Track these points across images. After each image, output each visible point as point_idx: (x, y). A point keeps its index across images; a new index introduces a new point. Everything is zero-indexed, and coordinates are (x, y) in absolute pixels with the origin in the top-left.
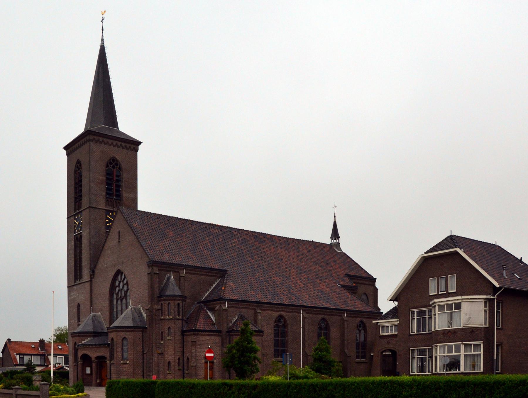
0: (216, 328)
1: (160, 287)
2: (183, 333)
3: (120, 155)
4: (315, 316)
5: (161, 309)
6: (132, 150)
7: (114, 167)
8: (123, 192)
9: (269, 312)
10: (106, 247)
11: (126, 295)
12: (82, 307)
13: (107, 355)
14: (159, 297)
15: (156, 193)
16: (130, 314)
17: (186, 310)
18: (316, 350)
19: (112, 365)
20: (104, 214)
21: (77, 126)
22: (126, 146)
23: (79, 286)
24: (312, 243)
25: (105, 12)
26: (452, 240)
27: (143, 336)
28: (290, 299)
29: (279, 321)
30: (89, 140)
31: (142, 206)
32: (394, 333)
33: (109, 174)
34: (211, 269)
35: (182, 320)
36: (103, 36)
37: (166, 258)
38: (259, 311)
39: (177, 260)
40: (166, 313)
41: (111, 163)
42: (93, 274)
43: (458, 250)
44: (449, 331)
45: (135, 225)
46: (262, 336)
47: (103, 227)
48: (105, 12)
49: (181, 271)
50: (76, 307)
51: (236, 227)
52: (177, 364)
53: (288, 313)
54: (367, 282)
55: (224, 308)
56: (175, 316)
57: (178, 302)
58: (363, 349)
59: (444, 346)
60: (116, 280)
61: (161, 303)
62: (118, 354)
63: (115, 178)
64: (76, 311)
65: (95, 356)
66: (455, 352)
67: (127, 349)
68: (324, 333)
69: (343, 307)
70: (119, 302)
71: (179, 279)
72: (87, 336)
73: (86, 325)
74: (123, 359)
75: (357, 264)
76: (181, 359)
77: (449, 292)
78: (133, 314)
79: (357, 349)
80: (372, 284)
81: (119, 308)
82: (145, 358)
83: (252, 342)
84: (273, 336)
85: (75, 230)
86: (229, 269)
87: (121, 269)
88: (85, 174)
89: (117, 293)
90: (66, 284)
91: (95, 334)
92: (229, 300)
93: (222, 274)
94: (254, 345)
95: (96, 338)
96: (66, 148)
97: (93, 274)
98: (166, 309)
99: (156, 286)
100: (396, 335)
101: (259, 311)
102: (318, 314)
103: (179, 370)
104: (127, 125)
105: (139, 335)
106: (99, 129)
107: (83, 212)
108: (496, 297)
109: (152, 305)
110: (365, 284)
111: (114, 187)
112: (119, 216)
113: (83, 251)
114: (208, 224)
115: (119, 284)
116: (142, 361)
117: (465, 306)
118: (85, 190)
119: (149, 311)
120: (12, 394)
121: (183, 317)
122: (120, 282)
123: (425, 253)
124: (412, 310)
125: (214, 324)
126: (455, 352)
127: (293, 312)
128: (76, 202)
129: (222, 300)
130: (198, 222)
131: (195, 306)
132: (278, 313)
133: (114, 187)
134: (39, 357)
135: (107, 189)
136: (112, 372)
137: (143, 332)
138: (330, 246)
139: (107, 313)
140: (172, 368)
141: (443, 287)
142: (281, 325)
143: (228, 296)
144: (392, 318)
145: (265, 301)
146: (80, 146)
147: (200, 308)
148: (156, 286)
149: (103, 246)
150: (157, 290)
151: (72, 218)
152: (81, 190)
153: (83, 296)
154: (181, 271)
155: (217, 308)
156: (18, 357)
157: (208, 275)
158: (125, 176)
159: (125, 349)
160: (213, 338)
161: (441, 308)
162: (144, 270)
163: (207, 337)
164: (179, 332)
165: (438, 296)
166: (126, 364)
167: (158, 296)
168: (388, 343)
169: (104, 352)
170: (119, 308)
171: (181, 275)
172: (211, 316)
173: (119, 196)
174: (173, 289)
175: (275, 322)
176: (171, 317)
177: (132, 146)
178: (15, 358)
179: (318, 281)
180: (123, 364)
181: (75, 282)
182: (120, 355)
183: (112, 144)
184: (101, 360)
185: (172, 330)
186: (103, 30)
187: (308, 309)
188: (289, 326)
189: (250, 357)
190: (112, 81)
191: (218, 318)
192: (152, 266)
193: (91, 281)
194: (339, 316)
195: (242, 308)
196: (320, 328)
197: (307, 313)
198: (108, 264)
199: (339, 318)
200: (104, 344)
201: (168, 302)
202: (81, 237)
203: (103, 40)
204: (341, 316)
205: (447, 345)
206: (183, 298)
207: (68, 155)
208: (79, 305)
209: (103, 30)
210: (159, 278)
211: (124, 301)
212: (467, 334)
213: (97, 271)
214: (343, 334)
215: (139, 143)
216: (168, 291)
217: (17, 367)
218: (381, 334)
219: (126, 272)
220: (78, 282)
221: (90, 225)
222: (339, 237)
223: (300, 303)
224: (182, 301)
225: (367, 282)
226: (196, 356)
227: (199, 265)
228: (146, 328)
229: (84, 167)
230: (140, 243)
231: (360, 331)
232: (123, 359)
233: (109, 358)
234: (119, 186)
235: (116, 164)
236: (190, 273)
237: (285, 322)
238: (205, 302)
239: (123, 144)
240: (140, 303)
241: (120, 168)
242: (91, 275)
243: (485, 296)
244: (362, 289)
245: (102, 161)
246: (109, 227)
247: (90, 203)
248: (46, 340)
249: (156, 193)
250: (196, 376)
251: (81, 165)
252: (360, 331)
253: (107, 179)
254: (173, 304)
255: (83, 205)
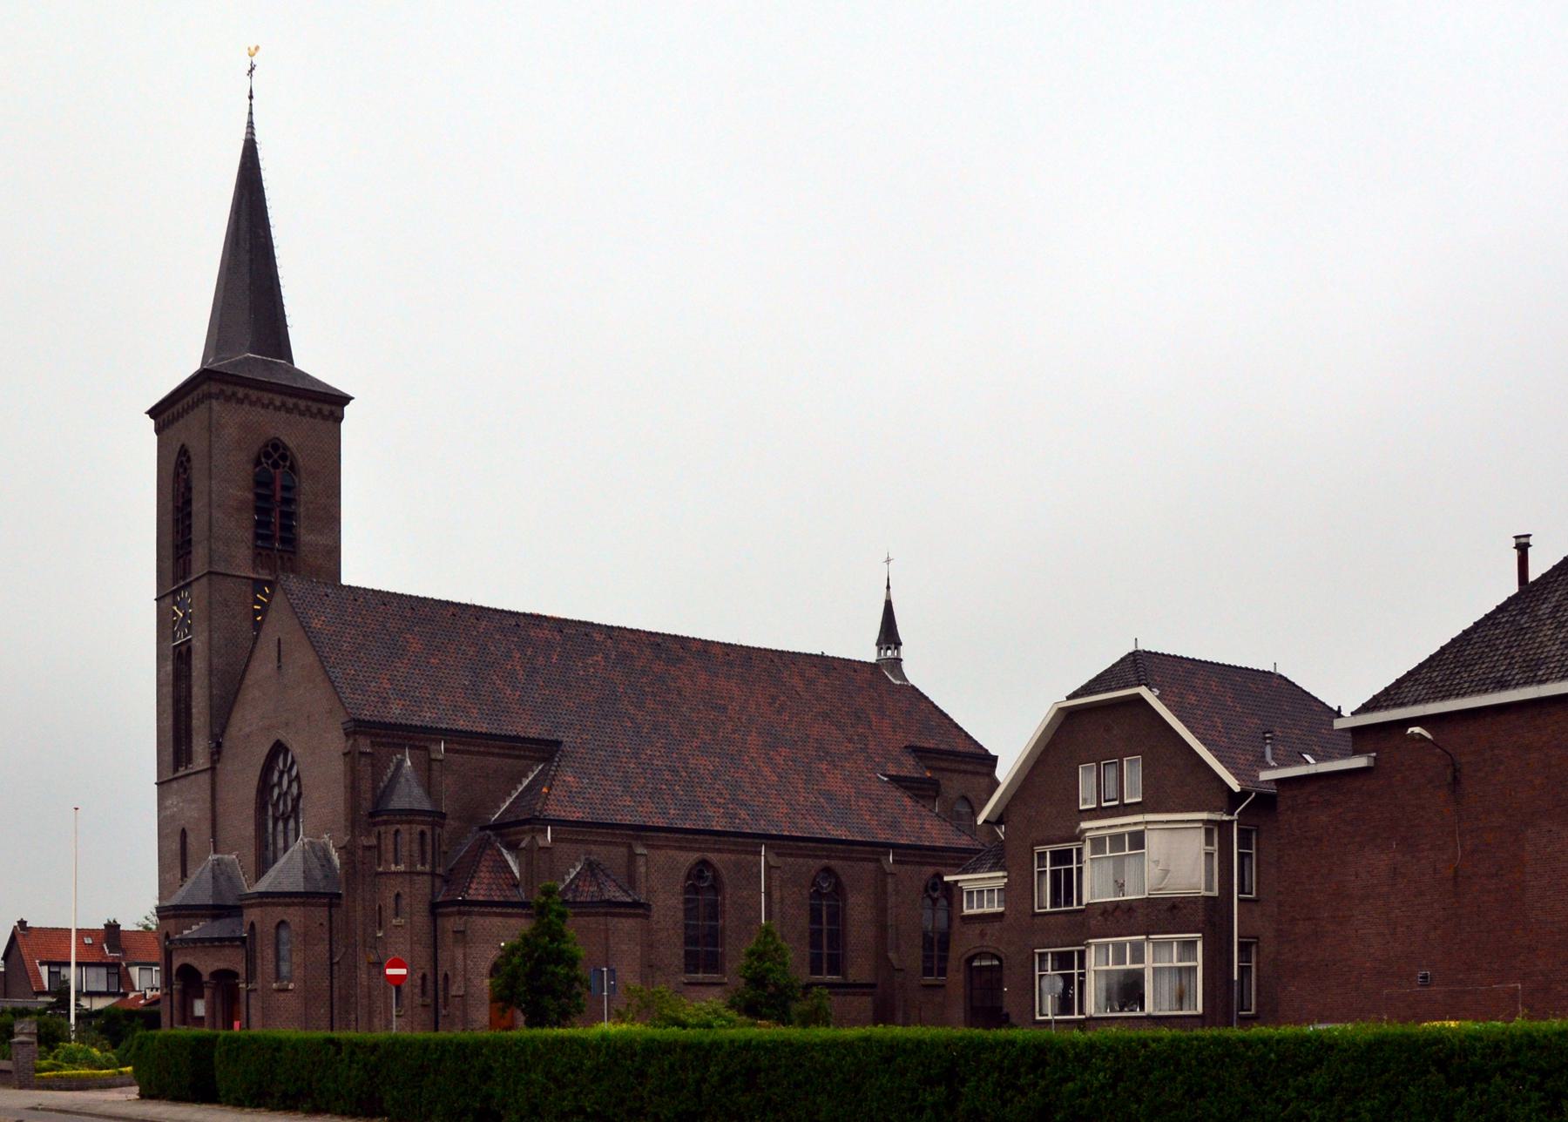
0: (520, 895)
1: (374, 789)
2: (435, 909)
3: (293, 432)
4: (801, 860)
5: (378, 847)
6: (325, 418)
7: (275, 465)
8: (302, 531)
9: (671, 853)
10: (247, 682)
11: (295, 808)
12: (191, 839)
13: (241, 969)
14: (371, 815)
15: (394, 534)
16: (298, 858)
17: (444, 848)
18: (751, 954)
19: (252, 995)
20: (249, 590)
21: (181, 354)
22: (308, 409)
23: (183, 782)
24: (822, 658)
25: (257, 48)
26: (1139, 665)
27: (331, 916)
28: (735, 816)
29: (700, 877)
30: (209, 396)
31: (358, 570)
32: (997, 909)
33: (262, 483)
34: (517, 738)
35: (433, 874)
36: (251, 113)
37: (395, 712)
38: (640, 850)
39: (427, 717)
40: (390, 856)
41: (268, 455)
42: (217, 751)
43: (1143, 691)
44: (1117, 905)
45: (316, 624)
46: (647, 917)
47: (247, 625)
48: (257, 48)
49: (433, 747)
50: (178, 839)
51: (603, 622)
52: (417, 991)
53: (726, 856)
54: (970, 768)
55: (541, 843)
56: (412, 864)
57: (419, 828)
58: (937, 947)
59: (1107, 945)
60: (273, 769)
61: (376, 830)
62: (265, 965)
63: (278, 496)
64: (177, 851)
65: (210, 970)
66: (1133, 962)
67: (290, 951)
68: (829, 906)
69: (882, 837)
70: (281, 825)
71: (427, 768)
72: (196, 916)
73: (197, 889)
74: (278, 978)
75: (946, 716)
76: (430, 977)
77: (1127, 801)
78: (305, 860)
79: (924, 948)
80: (985, 770)
81: (281, 843)
82: (336, 974)
83: (563, 936)
84: (681, 915)
85: (174, 634)
86: (566, 738)
87: (283, 740)
88: (199, 485)
89: (275, 805)
90: (152, 776)
91: (217, 911)
92: (557, 823)
93: (547, 750)
94: (564, 946)
95: (217, 923)
96: (153, 413)
97: (217, 751)
98: (391, 847)
99: (365, 785)
100: (1001, 914)
101: (640, 850)
102: (809, 856)
103: (424, 1006)
104: (314, 353)
105: (320, 914)
106: (236, 365)
107: (195, 586)
108: (1236, 816)
109: (353, 836)
110: (965, 772)
111: (275, 519)
112: (279, 597)
113: (195, 690)
114: (524, 615)
115: (281, 777)
116: (328, 983)
117: (1153, 840)
118: (199, 524)
119: (347, 851)
120: (9, 1072)
121: (433, 866)
122: (281, 774)
123: (1069, 698)
124: (1038, 849)
125: (516, 886)
126: (1133, 962)
127: (739, 852)
128: (177, 558)
129: (538, 822)
130: (496, 610)
131: (469, 840)
132: (693, 857)
133: (275, 519)
134: (103, 971)
135: (258, 524)
136: (252, 1011)
137: (331, 906)
138: (874, 668)
139: (251, 858)
140: (406, 1002)
141: (1111, 791)
142: (703, 885)
143: (554, 810)
144: (990, 870)
145: (661, 822)
146: (186, 411)
147: (485, 844)
148: (365, 785)
149: (242, 678)
150: (369, 796)
151: (169, 600)
152: (189, 526)
153: (193, 811)
154: (433, 747)
155: (523, 845)
156: (44, 971)
157: (509, 756)
158: (307, 489)
159: (284, 950)
160: (512, 921)
161: (1098, 844)
162: (335, 742)
163: (498, 921)
164: (422, 908)
165: (1099, 813)
166: (287, 990)
167: (370, 812)
168: (982, 935)
169: (231, 960)
170: (281, 843)
171: (433, 756)
172: (512, 864)
173: (290, 540)
174: (409, 795)
175: (688, 877)
176: (402, 868)
177: (326, 408)
178: (38, 975)
179: (824, 766)
180: (279, 990)
181: (176, 770)
182: (271, 966)
183: (271, 403)
184: (225, 978)
185: (404, 902)
186: (251, 97)
187: (780, 843)
188: (728, 890)
189: (554, 974)
190: (274, 232)
191: (527, 867)
192: (355, 733)
193: (213, 769)
194: (870, 860)
195: (595, 843)
196: (818, 894)
197: (778, 854)
198: (252, 726)
199: (871, 866)
200: (232, 939)
201: (393, 828)
202: (189, 650)
203: (251, 125)
204: (878, 860)
205: (1114, 944)
206: (437, 818)
207: (158, 431)
208: (184, 833)
209: (251, 97)
210: (373, 765)
211: (292, 824)
212: (1161, 915)
213: (226, 744)
214: (882, 910)
215: (346, 399)
216: (395, 798)
217: (41, 999)
218: (966, 911)
219: (296, 749)
220: (182, 771)
221: (210, 619)
222: (898, 644)
223: (761, 827)
224: (433, 825)
225: (970, 768)
226: (465, 970)
227: (484, 727)
228: (339, 896)
229: (197, 464)
230: (326, 672)
231: (935, 901)
232: (278, 978)
233: (244, 976)
234: (289, 516)
235: (284, 457)
236: (457, 752)
237: (716, 877)
238: (498, 827)
239: (302, 404)
240: (326, 830)
241: (292, 467)
242: (212, 754)
243: (1204, 816)
244: (953, 785)
245: (248, 449)
246: (257, 627)
247: (210, 563)
248: (126, 925)
249: (394, 534)
250: (466, 1023)
251: (189, 460)
252: (935, 901)
253: (258, 496)
254: (409, 833)
255: (194, 566)
